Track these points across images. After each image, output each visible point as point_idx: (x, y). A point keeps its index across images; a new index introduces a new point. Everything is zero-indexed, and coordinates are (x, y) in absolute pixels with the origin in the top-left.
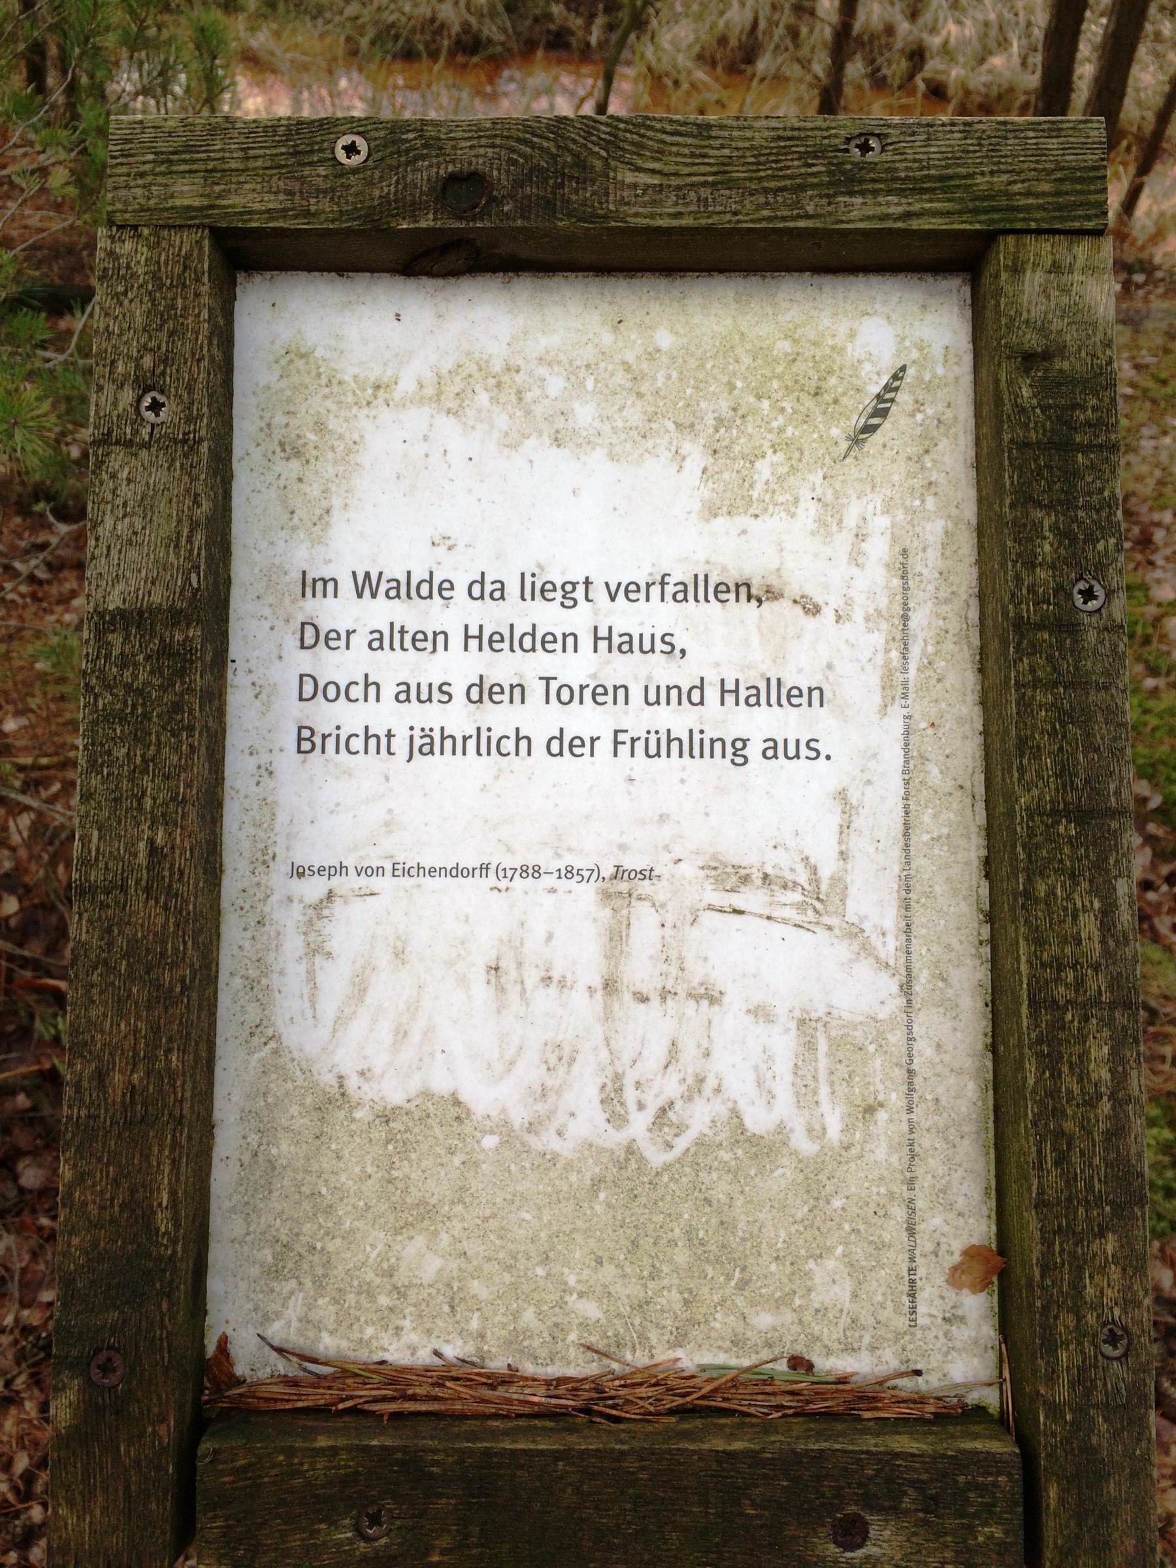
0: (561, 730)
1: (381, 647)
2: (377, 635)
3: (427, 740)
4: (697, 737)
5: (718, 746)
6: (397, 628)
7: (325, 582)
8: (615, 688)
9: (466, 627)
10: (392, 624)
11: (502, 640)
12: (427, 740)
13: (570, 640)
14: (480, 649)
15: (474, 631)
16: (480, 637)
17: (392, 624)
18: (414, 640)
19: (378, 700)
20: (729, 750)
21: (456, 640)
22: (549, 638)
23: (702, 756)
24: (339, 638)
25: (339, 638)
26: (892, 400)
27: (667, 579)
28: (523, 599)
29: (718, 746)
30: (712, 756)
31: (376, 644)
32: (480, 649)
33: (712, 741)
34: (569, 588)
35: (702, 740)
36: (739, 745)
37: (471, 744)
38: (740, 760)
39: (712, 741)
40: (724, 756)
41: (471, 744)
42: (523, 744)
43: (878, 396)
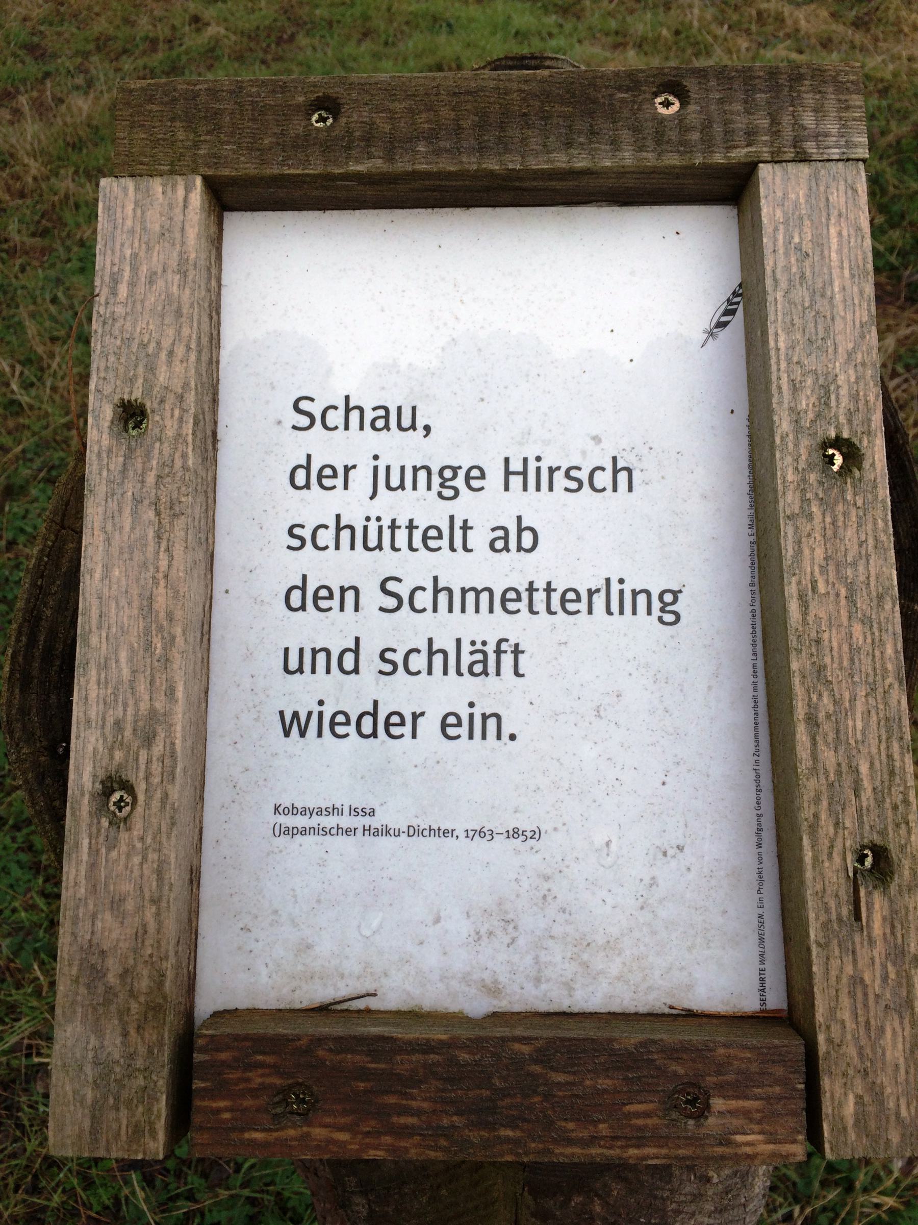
0: (304, 577)
1: (506, 548)
2: (501, 533)
3: (479, 657)
4: (615, 588)
5: (642, 599)
6: (458, 523)
7: (478, 593)
8: (343, 590)
9: (507, 460)
10: (452, 518)
11: (440, 537)
12: (479, 657)
13: (350, 595)
14: (525, 488)
15: (516, 466)
16: (524, 473)
17: (452, 518)
18: (425, 538)
19: (630, 489)
20: (656, 605)
21: (495, 475)
22: (395, 719)
23: (621, 612)
24: (331, 597)
25: (331, 597)
26: (738, 303)
27: (504, 646)
28: (609, 612)
29: (642, 599)
30: (634, 612)
31: (499, 544)
32: (525, 488)
33: (635, 593)
34: (448, 474)
35: (621, 592)
36: (668, 598)
37: (599, 601)
38: (669, 618)
39: (635, 593)
40: (649, 613)
41: (599, 601)
42: (623, 477)
43: (728, 300)
